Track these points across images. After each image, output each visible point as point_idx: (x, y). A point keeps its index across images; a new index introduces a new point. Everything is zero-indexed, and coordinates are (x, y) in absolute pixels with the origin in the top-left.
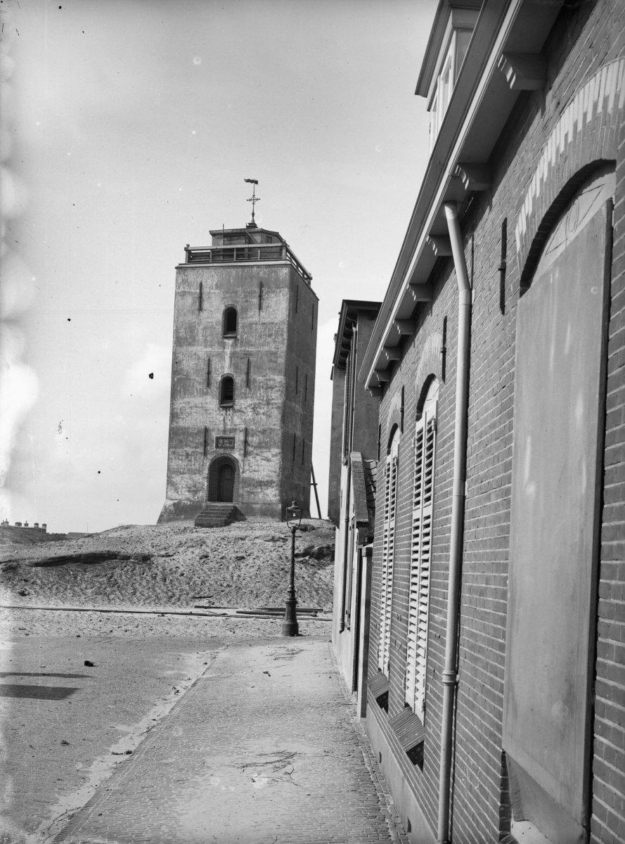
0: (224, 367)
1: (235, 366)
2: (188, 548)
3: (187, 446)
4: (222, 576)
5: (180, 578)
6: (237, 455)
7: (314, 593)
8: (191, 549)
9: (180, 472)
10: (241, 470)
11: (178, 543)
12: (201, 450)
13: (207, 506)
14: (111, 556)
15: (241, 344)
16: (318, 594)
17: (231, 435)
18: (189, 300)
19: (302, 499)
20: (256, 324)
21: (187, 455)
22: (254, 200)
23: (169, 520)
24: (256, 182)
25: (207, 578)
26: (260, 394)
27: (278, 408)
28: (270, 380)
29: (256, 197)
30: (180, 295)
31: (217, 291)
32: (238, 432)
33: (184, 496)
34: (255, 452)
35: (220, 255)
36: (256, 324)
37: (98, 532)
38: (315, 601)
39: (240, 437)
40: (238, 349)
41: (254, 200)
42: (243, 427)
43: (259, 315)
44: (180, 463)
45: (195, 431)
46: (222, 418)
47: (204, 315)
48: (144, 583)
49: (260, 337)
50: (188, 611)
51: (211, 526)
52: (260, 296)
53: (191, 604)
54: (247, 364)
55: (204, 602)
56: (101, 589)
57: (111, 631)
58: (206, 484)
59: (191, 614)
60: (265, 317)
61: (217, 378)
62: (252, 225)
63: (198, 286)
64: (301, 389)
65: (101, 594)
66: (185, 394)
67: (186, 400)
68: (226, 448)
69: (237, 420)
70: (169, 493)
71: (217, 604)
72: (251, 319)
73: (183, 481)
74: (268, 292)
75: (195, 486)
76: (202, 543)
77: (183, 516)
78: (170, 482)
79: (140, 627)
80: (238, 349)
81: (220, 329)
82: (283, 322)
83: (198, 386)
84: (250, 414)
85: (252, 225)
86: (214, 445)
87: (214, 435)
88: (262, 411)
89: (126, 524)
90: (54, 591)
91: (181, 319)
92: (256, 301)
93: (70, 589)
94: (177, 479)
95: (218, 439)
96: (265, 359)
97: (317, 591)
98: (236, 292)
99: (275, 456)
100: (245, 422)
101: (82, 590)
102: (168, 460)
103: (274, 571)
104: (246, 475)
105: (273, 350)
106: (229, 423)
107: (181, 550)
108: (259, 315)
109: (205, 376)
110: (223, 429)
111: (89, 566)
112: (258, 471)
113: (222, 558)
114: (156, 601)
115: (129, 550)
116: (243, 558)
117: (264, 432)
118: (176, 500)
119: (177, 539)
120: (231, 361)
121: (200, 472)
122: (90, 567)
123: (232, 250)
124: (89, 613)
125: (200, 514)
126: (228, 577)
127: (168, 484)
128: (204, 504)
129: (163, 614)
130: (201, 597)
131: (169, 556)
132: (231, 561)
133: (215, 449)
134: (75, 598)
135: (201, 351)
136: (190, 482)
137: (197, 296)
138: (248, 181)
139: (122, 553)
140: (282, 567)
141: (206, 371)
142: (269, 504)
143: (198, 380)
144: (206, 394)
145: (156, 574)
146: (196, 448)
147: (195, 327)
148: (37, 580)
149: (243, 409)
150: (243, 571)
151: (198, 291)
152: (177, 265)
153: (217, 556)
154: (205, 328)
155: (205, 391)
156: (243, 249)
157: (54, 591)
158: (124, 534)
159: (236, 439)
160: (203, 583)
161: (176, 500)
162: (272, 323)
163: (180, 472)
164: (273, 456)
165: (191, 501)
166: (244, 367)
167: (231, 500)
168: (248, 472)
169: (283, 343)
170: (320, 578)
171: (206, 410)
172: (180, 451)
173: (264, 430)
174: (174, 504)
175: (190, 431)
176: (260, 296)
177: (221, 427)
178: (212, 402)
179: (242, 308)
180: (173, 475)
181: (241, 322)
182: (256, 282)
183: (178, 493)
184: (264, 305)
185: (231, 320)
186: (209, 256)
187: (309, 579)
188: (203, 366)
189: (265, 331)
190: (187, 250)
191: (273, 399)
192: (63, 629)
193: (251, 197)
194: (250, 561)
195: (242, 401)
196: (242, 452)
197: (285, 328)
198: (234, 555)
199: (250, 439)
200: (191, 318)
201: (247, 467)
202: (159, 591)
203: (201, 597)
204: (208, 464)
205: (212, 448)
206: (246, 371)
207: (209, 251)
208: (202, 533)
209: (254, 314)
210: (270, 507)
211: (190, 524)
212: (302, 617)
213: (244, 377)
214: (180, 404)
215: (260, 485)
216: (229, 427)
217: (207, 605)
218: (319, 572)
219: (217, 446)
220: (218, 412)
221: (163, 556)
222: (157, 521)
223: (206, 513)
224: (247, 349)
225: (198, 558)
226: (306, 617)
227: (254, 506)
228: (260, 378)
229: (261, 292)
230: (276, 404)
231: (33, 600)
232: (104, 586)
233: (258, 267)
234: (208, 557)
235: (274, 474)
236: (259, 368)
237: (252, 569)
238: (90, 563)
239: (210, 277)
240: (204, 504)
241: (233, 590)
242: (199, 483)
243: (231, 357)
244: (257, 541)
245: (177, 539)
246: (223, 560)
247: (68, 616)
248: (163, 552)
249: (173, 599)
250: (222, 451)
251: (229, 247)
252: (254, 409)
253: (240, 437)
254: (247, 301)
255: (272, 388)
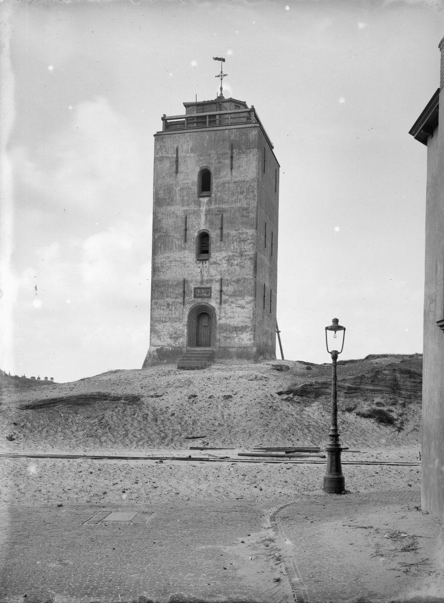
0: (200, 224)
1: (211, 223)
2: (175, 389)
3: (167, 297)
4: (212, 415)
5: (171, 418)
6: (213, 303)
7: (306, 431)
8: (179, 390)
9: (162, 321)
10: (218, 317)
11: (166, 384)
12: (180, 300)
13: (187, 351)
14: (103, 397)
15: (216, 202)
16: (310, 431)
17: (208, 286)
18: (167, 164)
19: (270, 344)
20: (229, 183)
21: (168, 305)
22: (222, 76)
23: (153, 365)
24: (223, 60)
25: (198, 418)
26: (234, 247)
27: (251, 259)
28: (242, 233)
29: (219, 78)
30: (158, 160)
31: (192, 155)
32: (214, 283)
33: (166, 342)
34: (230, 300)
35: (194, 123)
36: (229, 183)
37: (90, 377)
38: (309, 439)
39: (216, 287)
40: (213, 207)
41: (222, 76)
42: (219, 277)
43: (232, 175)
44: (162, 313)
45: (175, 283)
46: (199, 270)
47: (180, 176)
48: (136, 424)
49: (233, 194)
50: (186, 453)
51: (193, 369)
52: (232, 157)
53: (185, 444)
54: (220, 218)
55: (198, 443)
56: (93, 431)
57: (105, 493)
58: (186, 331)
59: (190, 458)
60: (237, 176)
61: (194, 234)
62: (221, 97)
63: (175, 151)
64: (268, 244)
65: (93, 436)
66: (165, 250)
67: (166, 255)
68: (203, 297)
69: (213, 272)
70: (152, 340)
71: (211, 445)
72: (224, 179)
73: (165, 329)
74: (239, 153)
75: (175, 333)
76: (189, 382)
77: (165, 361)
78: (153, 330)
79: (140, 484)
80: (213, 207)
81: (196, 189)
82: (253, 180)
83: (177, 242)
84: (225, 265)
85: (221, 97)
86: (193, 295)
87: (192, 286)
88: (235, 262)
89: (114, 370)
90: (44, 434)
91: (160, 182)
92: (228, 162)
93: (60, 432)
94: (159, 327)
95: (195, 289)
96: (238, 214)
97: (308, 428)
98: (210, 155)
99: (250, 303)
100: (221, 273)
101: (73, 432)
102: (151, 310)
103: (263, 409)
104: (223, 321)
105: (245, 206)
106: (205, 274)
107: (169, 390)
108: (232, 175)
109: (183, 233)
110: (200, 280)
111: (80, 407)
112: (234, 318)
113: (210, 397)
114: (149, 442)
115: (119, 391)
116: (230, 397)
117: (238, 281)
118: (159, 346)
119: (163, 381)
120: (206, 218)
121: (180, 319)
122: (81, 409)
123: (205, 117)
124: (79, 460)
125: (181, 358)
126: (218, 416)
127: (151, 332)
128: (184, 350)
129: (161, 460)
130: (194, 438)
131: (158, 396)
132: (219, 400)
133: (193, 299)
134: (65, 442)
135: (178, 209)
136: (171, 329)
137: (174, 160)
138: (217, 59)
139: (112, 395)
140: (270, 405)
141: (184, 228)
142: (244, 348)
143: (176, 236)
144: (185, 249)
145: (147, 415)
146: (176, 298)
147: (173, 188)
148: (28, 423)
149: (218, 262)
150: (232, 411)
151: (175, 155)
152: (155, 133)
153: (205, 396)
154: (182, 189)
155: (183, 246)
156: (214, 116)
157: (44, 434)
158: (113, 377)
159: (213, 290)
160: (194, 422)
161: (159, 346)
162: (244, 181)
163: (162, 321)
164: (247, 303)
165: (172, 347)
166: (218, 222)
167: (209, 345)
168: (224, 319)
169: (255, 200)
170: (308, 416)
171: (185, 264)
172: (160, 301)
173: (238, 280)
174: (157, 350)
175: (170, 283)
176: (232, 157)
177: (199, 278)
178: (190, 255)
179: (216, 169)
180: (156, 324)
181: (215, 182)
182: (227, 144)
183: (160, 339)
184: (235, 164)
185: (205, 181)
186: (184, 124)
187: (298, 417)
188: (181, 223)
189: (237, 188)
190: (164, 119)
191: (245, 251)
192: (43, 491)
193: (219, 73)
194: (236, 399)
195: (217, 254)
196: (218, 301)
197: (255, 184)
198: (222, 394)
199: (224, 288)
200: (169, 180)
201: (223, 314)
202: (151, 432)
203: (194, 438)
204: (187, 312)
205: (190, 298)
206: (220, 226)
207: (184, 119)
208: (186, 374)
209: (227, 174)
210: (245, 351)
211: (173, 367)
212: (310, 459)
213: (218, 231)
214: (160, 258)
215: (236, 330)
216: (205, 278)
217: (202, 446)
218: (307, 409)
219: (195, 296)
220: (195, 265)
221: (152, 397)
222: (425, 146)
223: (188, 357)
224: (221, 206)
225: (186, 398)
226: (314, 459)
227: (231, 350)
228: (233, 232)
229: (232, 153)
230: (248, 255)
231: (21, 445)
232: (95, 428)
233: (231, 132)
234: (196, 396)
235: (248, 320)
236: (232, 223)
237: (241, 408)
238: (81, 405)
239: (186, 142)
240: (184, 350)
241: (225, 430)
242: (180, 330)
243: (206, 215)
244: (241, 380)
245: (163, 381)
246: (211, 400)
247: (54, 465)
248: (152, 393)
249: (167, 440)
250: (199, 300)
251: (202, 114)
252: (229, 260)
253: (216, 287)
254: (219, 163)
255: (244, 241)
